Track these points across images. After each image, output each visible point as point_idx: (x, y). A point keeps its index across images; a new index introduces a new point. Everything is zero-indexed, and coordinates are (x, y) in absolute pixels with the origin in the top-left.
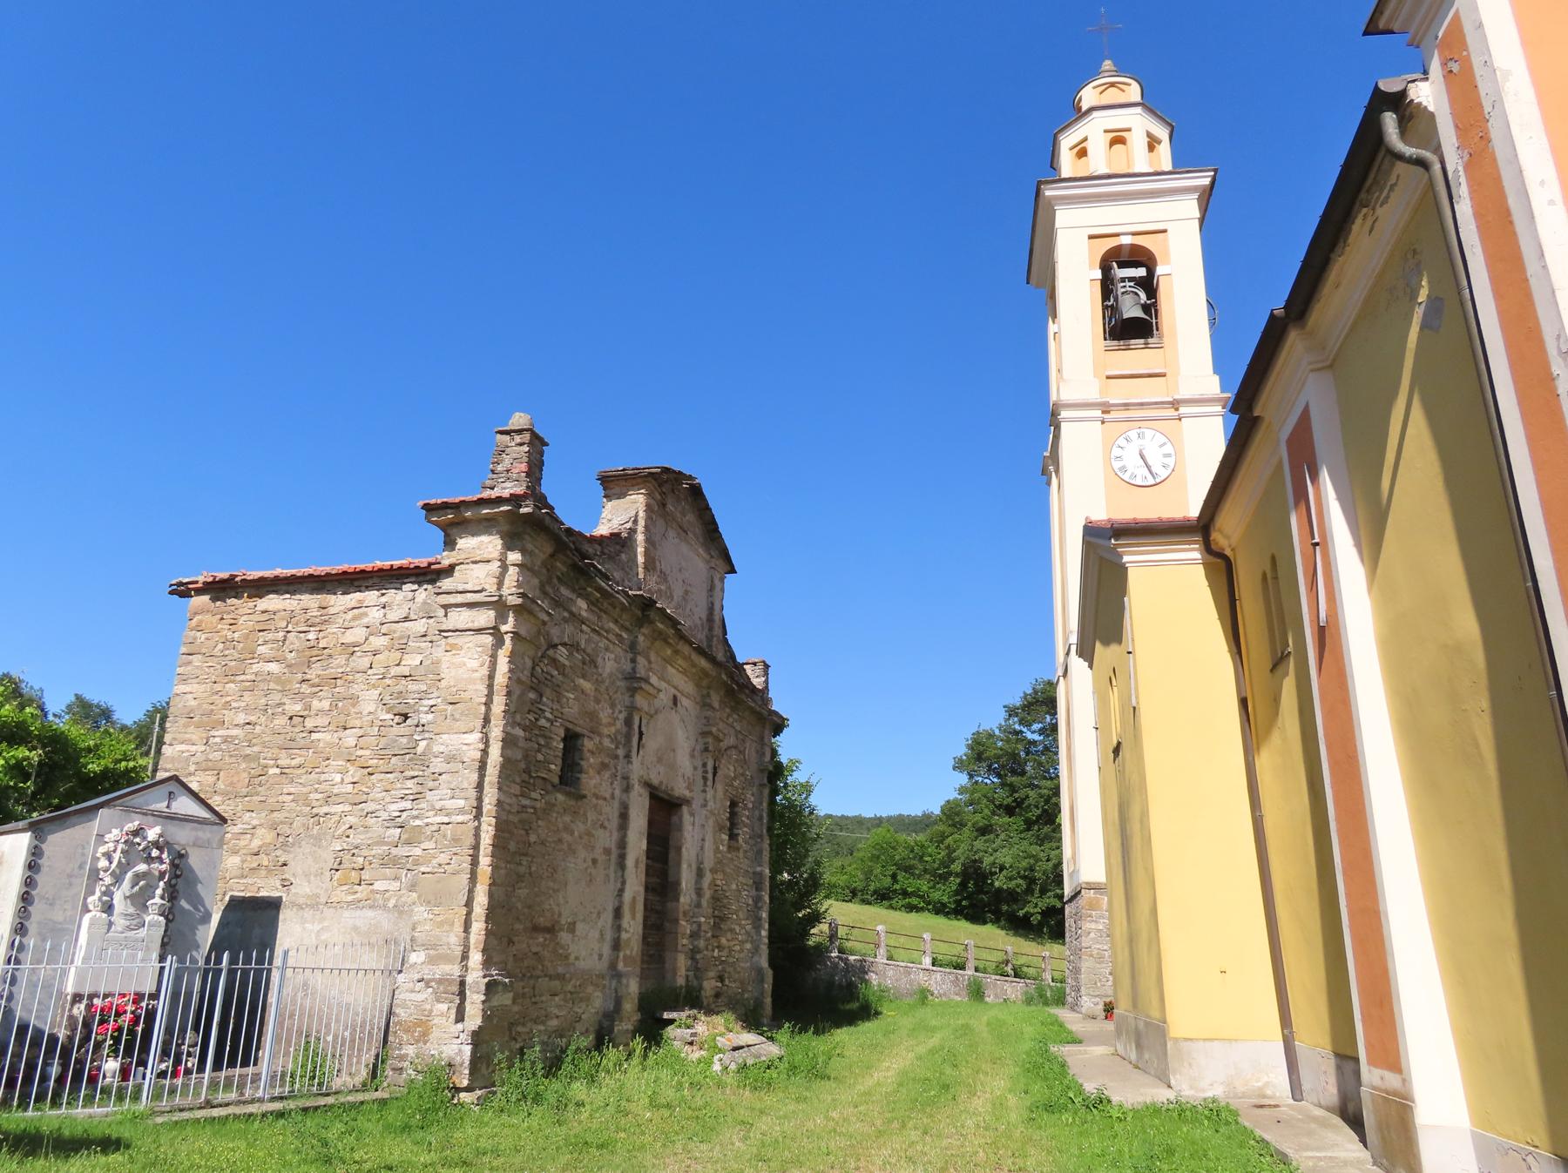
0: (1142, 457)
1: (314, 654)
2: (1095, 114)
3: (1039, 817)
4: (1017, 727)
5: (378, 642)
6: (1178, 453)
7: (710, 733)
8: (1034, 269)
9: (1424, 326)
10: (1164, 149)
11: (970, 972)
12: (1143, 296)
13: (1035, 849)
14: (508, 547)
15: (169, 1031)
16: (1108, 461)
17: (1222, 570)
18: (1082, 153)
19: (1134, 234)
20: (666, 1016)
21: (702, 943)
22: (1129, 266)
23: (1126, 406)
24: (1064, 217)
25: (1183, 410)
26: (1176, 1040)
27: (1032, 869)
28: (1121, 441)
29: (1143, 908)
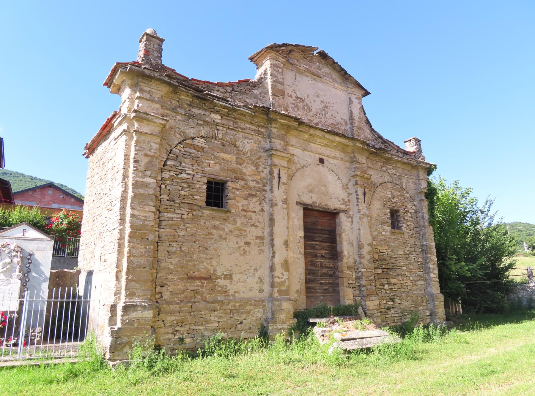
7: (356, 175)
15: (28, 328)
20: (312, 320)
21: (364, 282)
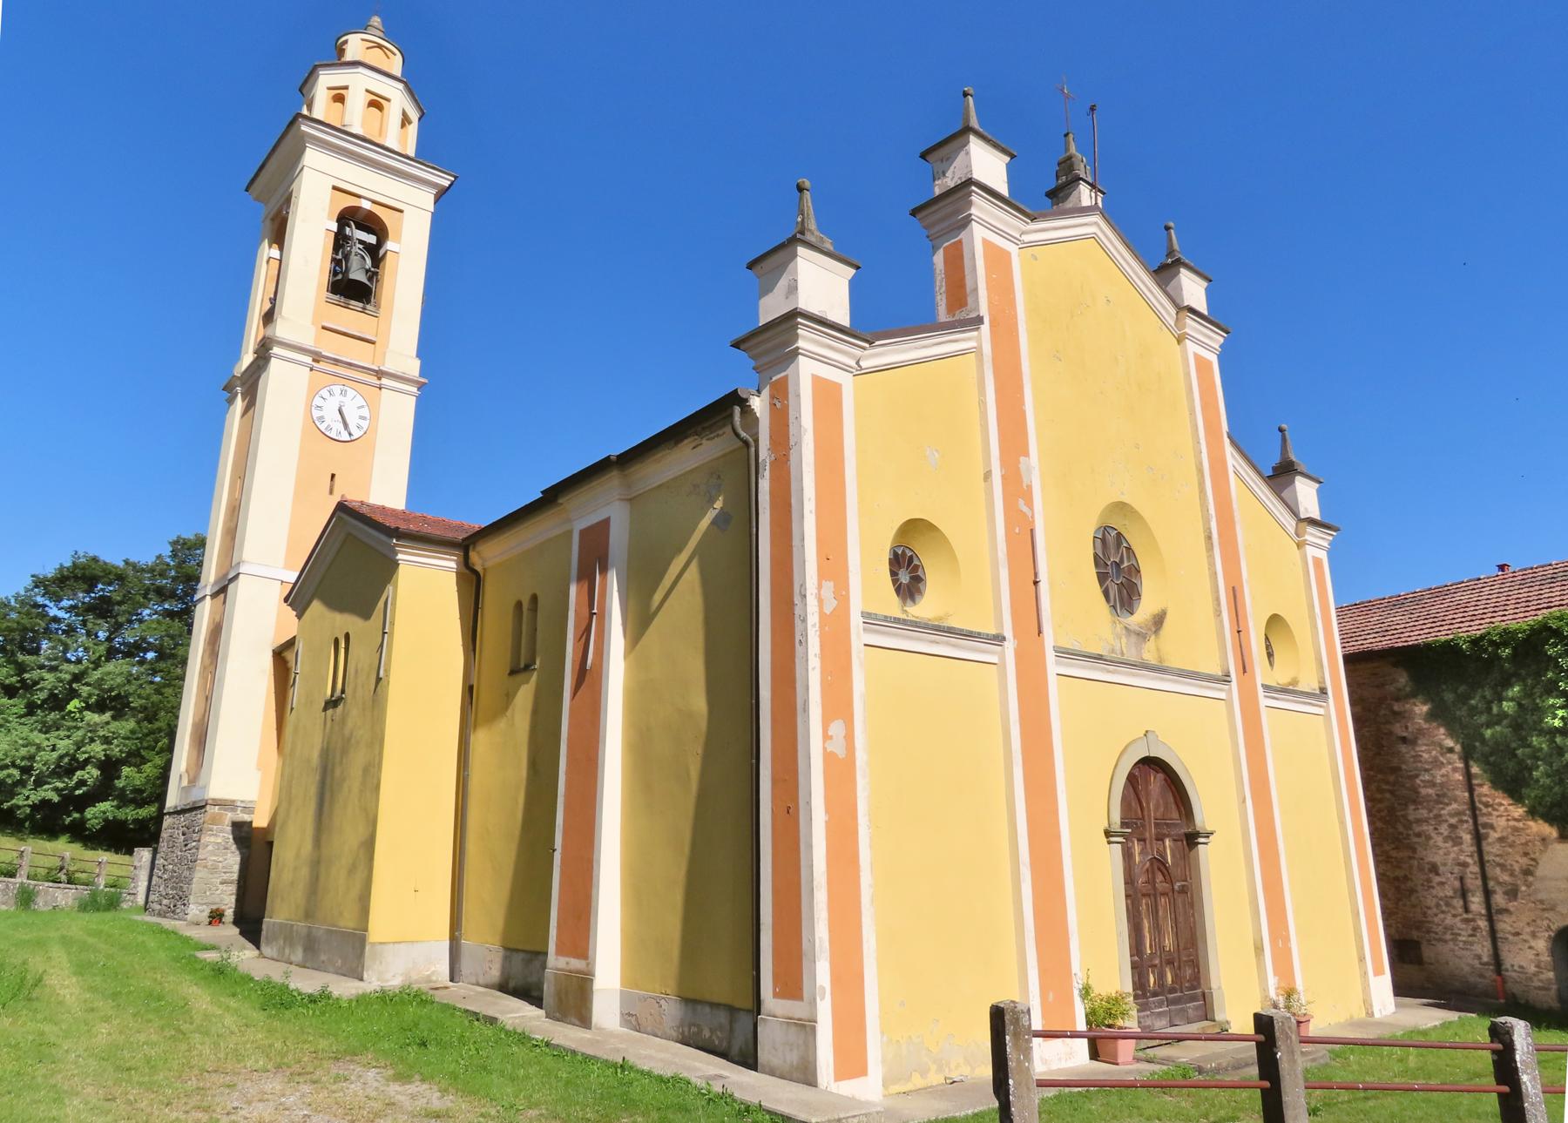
0: (340, 412)
2: (361, 69)
3: (44, 701)
4: (40, 600)
6: (374, 418)
8: (260, 179)
9: (714, 522)
10: (413, 129)
11: (21, 879)
12: (369, 261)
13: (38, 737)
16: (309, 406)
17: (472, 584)
18: (339, 99)
19: (374, 202)
22: (359, 230)
23: (336, 362)
24: (313, 158)
25: (385, 381)
26: (373, 944)
27: (32, 758)
28: (324, 393)
29: (347, 837)
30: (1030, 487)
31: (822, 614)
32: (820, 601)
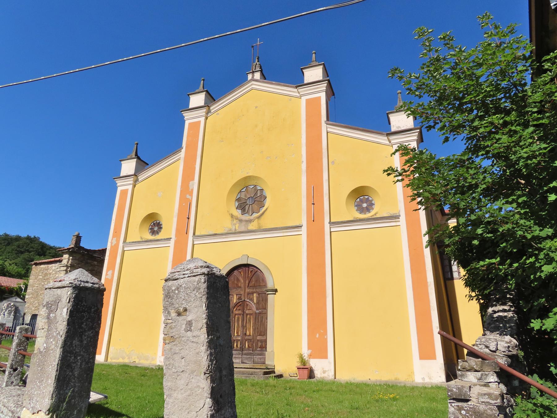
1: (46, 274)
5: (54, 272)
14: (70, 256)
30: (192, 190)
31: (111, 246)
32: (112, 243)
